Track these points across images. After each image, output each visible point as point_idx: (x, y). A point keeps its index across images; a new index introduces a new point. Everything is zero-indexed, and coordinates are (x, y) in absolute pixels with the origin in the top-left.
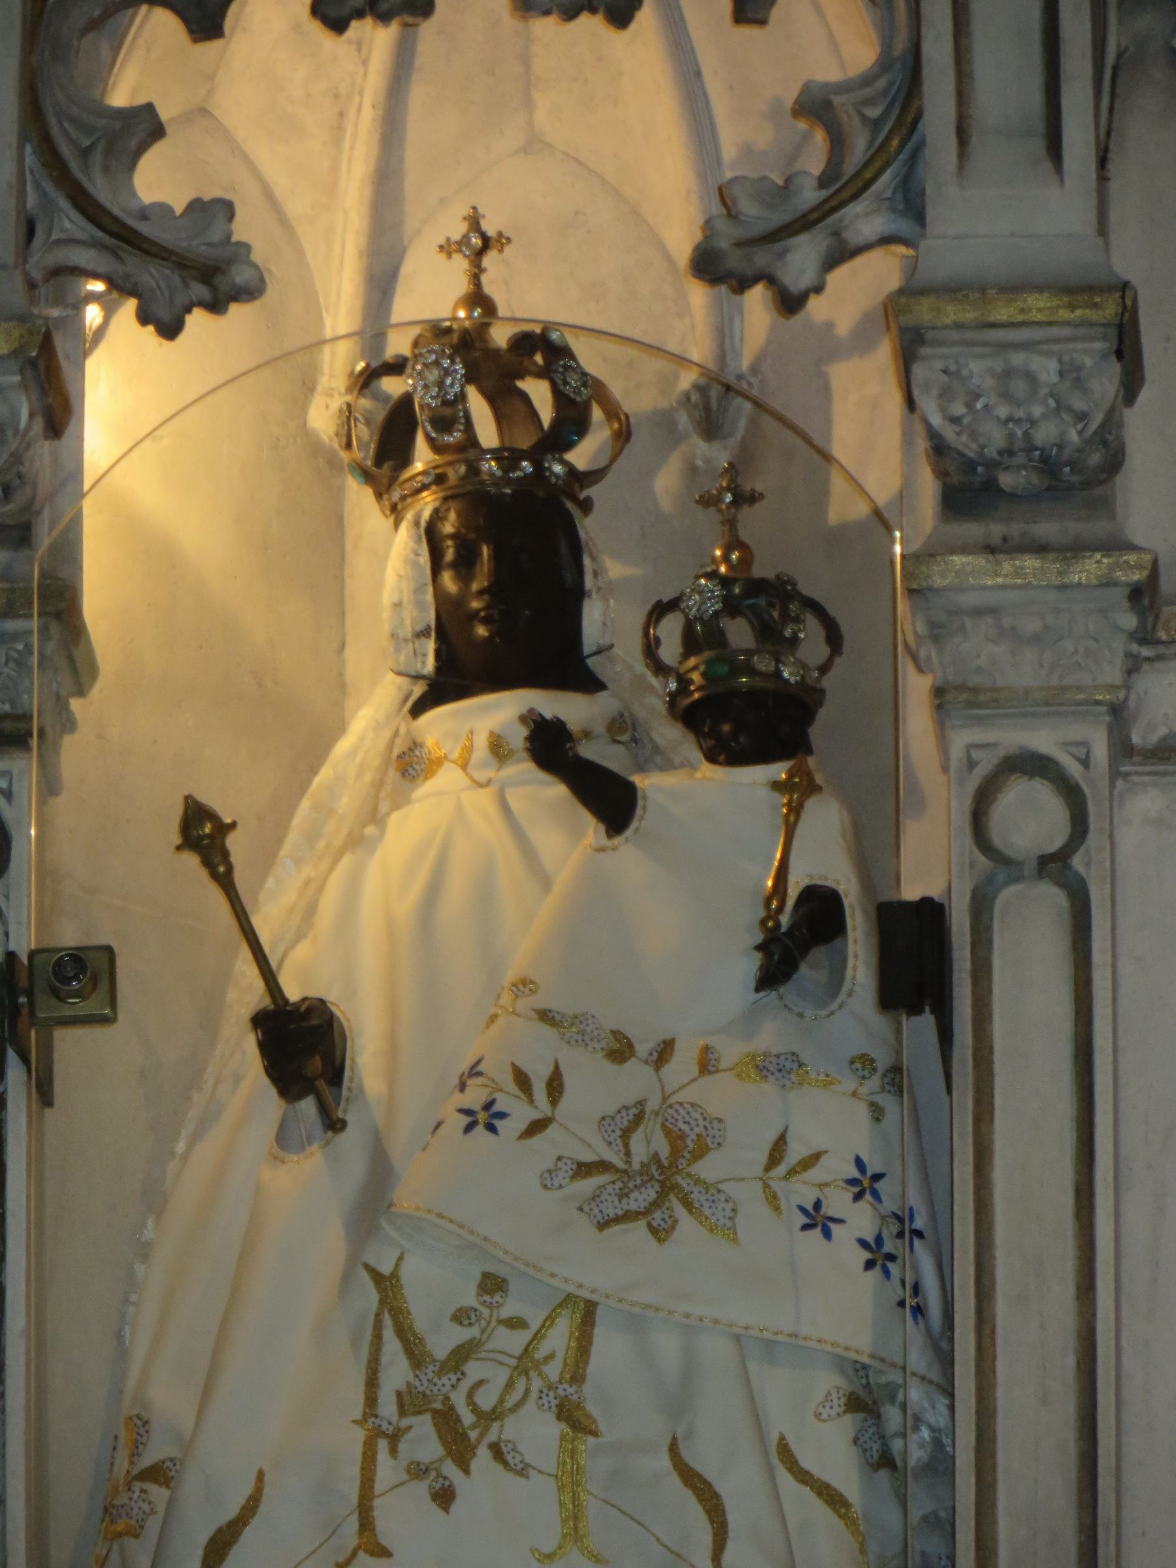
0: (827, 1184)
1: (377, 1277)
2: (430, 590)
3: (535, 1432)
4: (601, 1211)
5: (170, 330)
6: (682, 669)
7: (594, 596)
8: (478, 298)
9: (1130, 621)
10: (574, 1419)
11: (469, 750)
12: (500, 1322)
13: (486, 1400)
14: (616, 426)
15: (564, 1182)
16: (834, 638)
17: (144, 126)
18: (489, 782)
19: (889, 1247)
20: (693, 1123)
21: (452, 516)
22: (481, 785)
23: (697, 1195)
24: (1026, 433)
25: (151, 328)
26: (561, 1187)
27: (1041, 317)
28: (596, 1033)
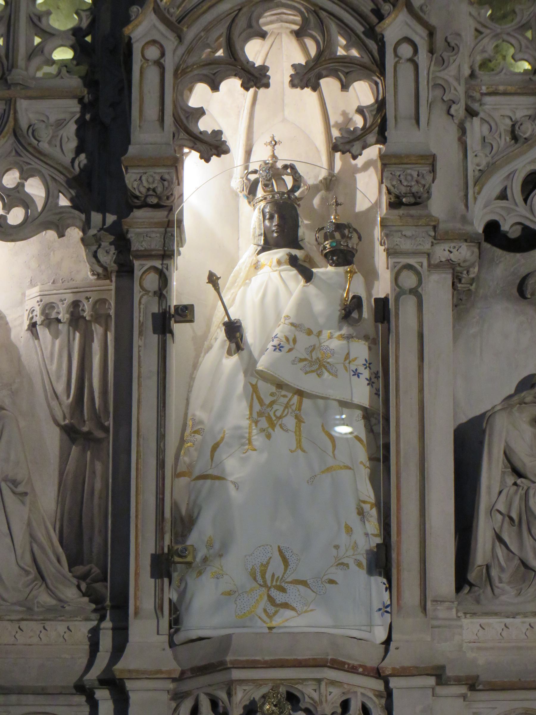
1: (251, 384)
3: (290, 422)
5: (207, 160)
8: (274, 156)
9: (432, 234)
10: (299, 420)
11: (272, 262)
12: (281, 396)
13: (278, 414)
16: (360, 238)
17: (200, 112)
19: (373, 380)
21: (268, 207)
23: (328, 366)
24: (410, 189)
25: (203, 160)
27: (414, 162)
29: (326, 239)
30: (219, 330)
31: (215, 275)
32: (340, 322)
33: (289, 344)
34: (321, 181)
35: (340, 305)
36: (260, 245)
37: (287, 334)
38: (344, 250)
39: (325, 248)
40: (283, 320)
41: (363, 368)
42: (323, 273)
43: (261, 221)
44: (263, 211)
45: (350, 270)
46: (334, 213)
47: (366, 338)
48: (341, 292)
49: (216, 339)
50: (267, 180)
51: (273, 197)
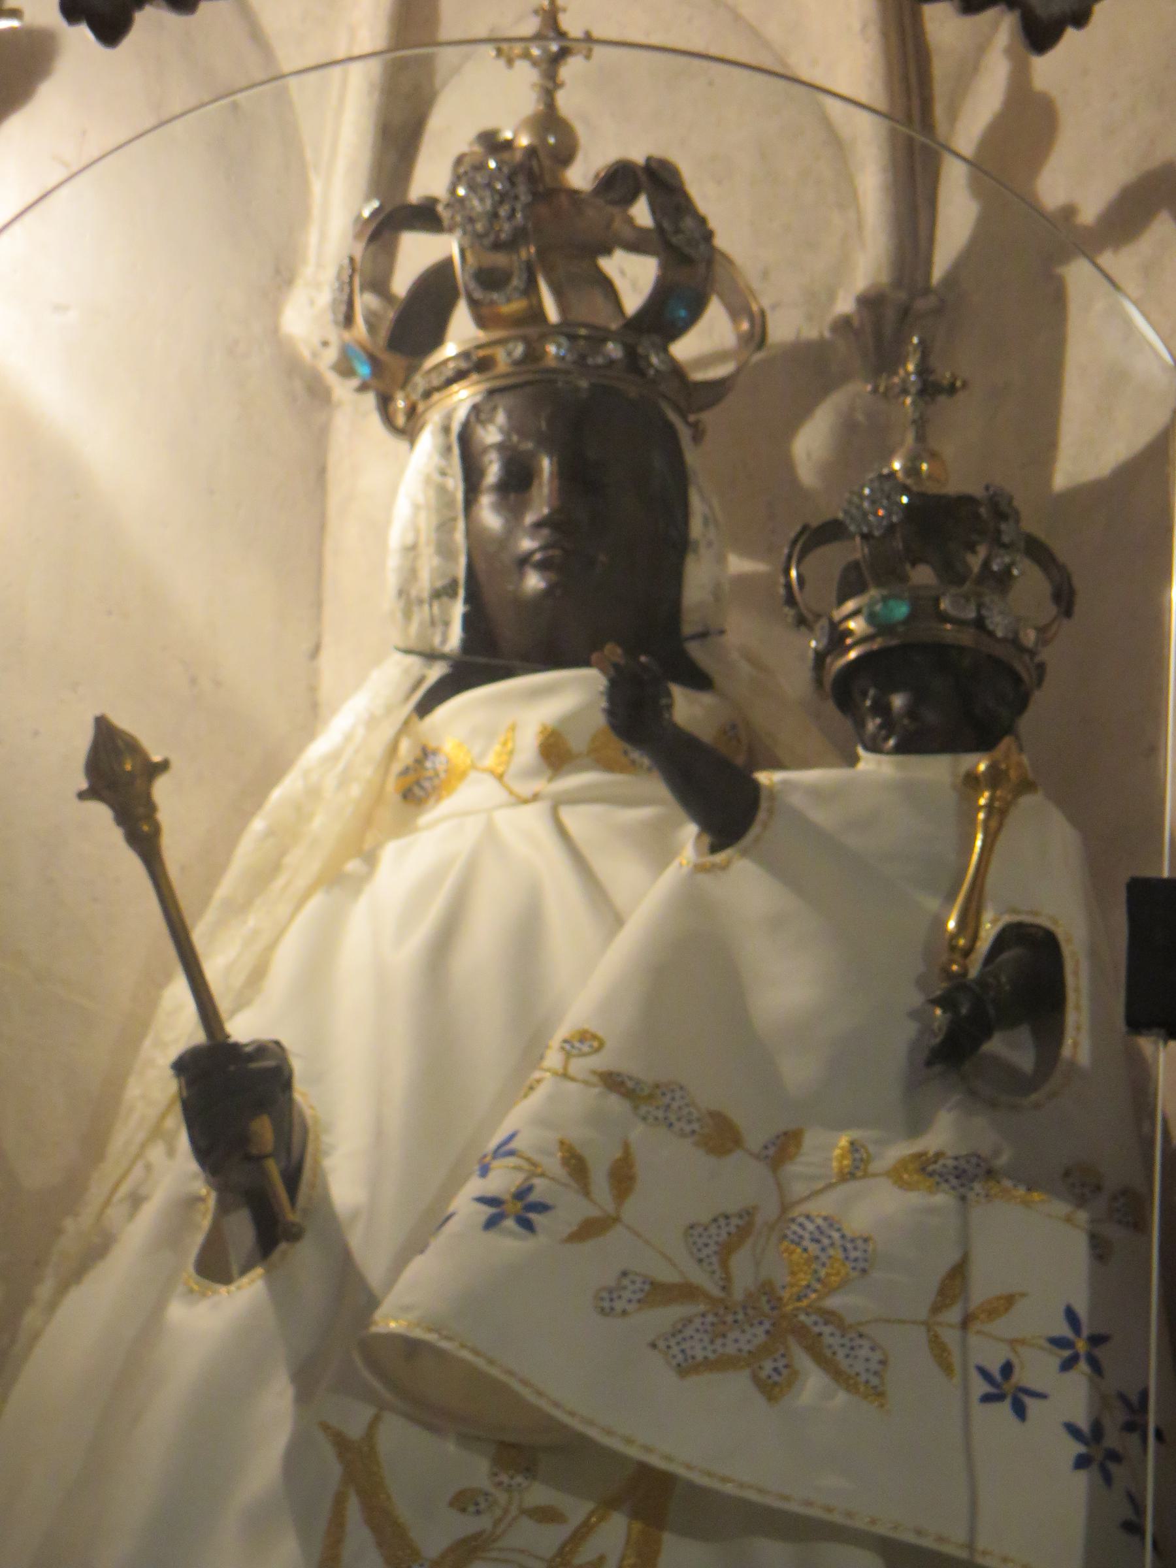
0: (1023, 1342)
1: (341, 1443)
2: (461, 525)
4: (683, 1351)
6: (837, 615)
7: (703, 550)
14: (745, 326)
15: (630, 1308)
16: (1064, 598)
18: (535, 797)
19: (1112, 1439)
20: (826, 1241)
21: (501, 418)
22: (525, 801)
26: (624, 1313)
28: (685, 1111)
29: (851, 584)
30: (156, 1153)
31: (133, 747)
32: (913, 1085)
33: (586, 1191)
34: (843, 325)
35: (921, 983)
36: (443, 657)
37: (577, 1134)
38: (961, 649)
39: (838, 639)
40: (553, 1059)
41: (1053, 1360)
42: (816, 793)
43: (450, 504)
44: (466, 438)
45: (992, 767)
46: (910, 438)
47: (1080, 1183)
48: (933, 904)
49: (136, 1201)
50: (497, 246)
51: (533, 355)
